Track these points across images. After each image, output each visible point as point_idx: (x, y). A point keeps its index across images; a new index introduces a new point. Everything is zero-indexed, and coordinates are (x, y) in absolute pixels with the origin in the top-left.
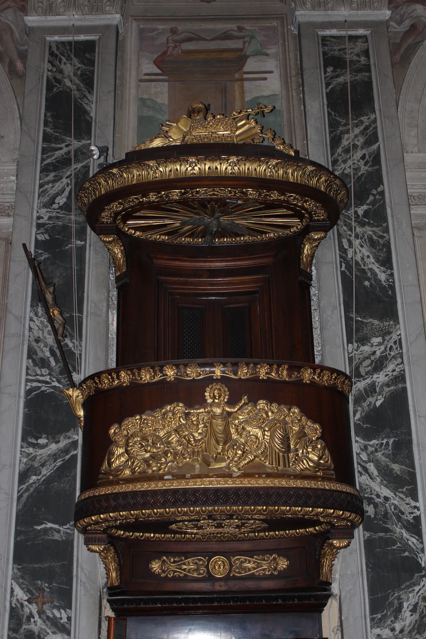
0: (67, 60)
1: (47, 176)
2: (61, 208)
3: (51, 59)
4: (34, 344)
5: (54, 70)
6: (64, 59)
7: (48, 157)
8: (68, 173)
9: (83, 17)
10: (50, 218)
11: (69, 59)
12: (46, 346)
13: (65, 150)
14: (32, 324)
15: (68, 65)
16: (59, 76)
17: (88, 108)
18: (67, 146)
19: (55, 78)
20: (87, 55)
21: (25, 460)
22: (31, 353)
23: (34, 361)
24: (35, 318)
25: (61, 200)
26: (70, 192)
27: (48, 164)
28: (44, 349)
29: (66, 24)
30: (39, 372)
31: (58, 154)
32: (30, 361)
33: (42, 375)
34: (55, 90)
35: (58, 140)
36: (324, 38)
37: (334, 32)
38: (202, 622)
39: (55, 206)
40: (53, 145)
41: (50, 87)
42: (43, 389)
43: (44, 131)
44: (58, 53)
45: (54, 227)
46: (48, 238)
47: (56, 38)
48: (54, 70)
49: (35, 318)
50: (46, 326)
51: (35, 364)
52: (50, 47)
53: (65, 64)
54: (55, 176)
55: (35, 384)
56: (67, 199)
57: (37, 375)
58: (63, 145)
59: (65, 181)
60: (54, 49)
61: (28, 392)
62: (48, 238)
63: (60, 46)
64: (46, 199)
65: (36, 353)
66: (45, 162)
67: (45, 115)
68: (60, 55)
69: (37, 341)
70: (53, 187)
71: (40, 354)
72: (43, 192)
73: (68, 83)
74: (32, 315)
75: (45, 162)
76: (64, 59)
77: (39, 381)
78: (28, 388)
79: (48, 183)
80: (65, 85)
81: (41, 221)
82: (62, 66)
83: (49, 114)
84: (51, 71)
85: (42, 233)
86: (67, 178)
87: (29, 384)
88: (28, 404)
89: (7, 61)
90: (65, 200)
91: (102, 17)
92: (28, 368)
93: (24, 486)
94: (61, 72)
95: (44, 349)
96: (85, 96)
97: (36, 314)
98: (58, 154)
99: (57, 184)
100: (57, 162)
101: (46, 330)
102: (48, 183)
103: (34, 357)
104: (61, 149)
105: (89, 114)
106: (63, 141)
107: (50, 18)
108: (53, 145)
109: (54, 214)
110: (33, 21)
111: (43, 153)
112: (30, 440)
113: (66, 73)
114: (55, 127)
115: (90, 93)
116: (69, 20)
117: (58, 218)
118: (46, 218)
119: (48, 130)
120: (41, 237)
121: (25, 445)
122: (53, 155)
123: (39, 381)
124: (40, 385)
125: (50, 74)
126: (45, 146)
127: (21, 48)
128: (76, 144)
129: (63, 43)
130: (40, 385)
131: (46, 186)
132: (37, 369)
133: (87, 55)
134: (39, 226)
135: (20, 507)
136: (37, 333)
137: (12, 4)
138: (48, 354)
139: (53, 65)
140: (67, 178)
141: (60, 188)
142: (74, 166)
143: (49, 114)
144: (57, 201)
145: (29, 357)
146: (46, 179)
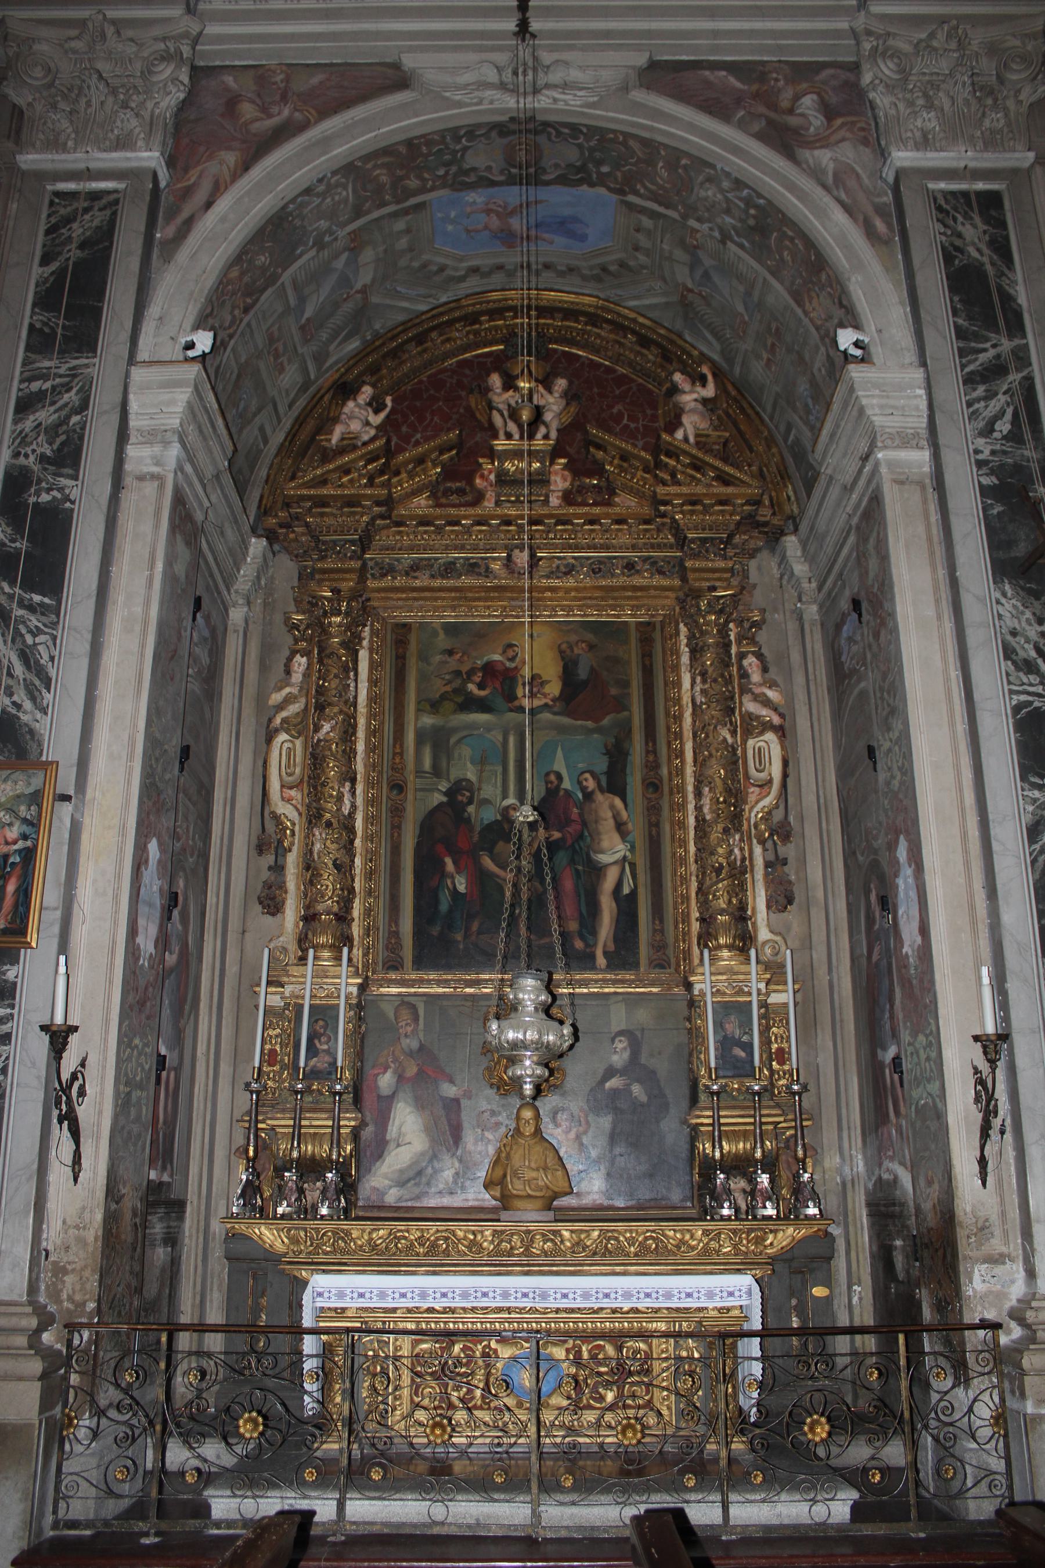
0: (965, 218)
1: (975, 390)
2: (1004, 438)
3: (940, 216)
4: (1009, 638)
5: (949, 232)
6: (960, 219)
7: (970, 362)
8: (1005, 387)
9: (979, 155)
10: (993, 453)
11: (967, 217)
12: (1028, 641)
13: (992, 353)
14: (1000, 608)
15: (968, 226)
16: (958, 242)
17: (1012, 291)
18: (994, 346)
19: (952, 244)
20: (993, 213)
21: (1030, 808)
22: (1008, 652)
23: (1014, 663)
24: (1003, 601)
25: (1003, 427)
26: (1016, 415)
27: (972, 373)
28: (1026, 646)
29: (954, 164)
30: (1025, 680)
31: (983, 357)
32: (1009, 663)
33: (1031, 685)
34: (957, 262)
35: (977, 337)
36: (57, 194)
37: (71, 186)
38: (116, 554)
39: (996, 435)
40: (973, 344)
41: (948, 258)
42: (1036, 704)
43: (955, 323)
44: (948, 207)
45: (1002, 466)
46: (996, 482)
47: (942, 185)
48: (949, 232)
49: (1003, 601)
50: (1023, 613)
51: (1018, 668)
52: (935, 199)
53: (963, 224)
54: (986, 391)
55: (1023, 698)
56: (1012, 424)
57: (1023, 684)
58: (988, 345)
59: (1002, 398)
60: (942, 202)
61: (1017, 709)
62: (996, 482)
63: (949, 197)
64: (981, 424)
65: (1014, 651)
66: (967, 370)
67: (951, 301)
68: (952, 212)
69: (1014, 633)
70: (986, 407)
71: (1022, 654)
72: (973, 413)
73: (975, 254)
74: (998, 595)
75: (967, 370)
76: (960, 219)
77: (1029, 693)
78: (1014, 703)
79: (978, 400)
80: (969, 256)
81: (980, 457)
82: (960, 228)
83: (956, 299)
84: (944, 234)
85: (987, 475)
86: (1005, 393)
87: (1015, 697)
88: (1020, 726)
89: (861, 218)
90: (1008, 427)
91: (1008, 155)
92: (1008, 674)
93: (1037, 846)
94: (960, 236)
95: (1026, 646)
96: (1003, 274)
97: (1004, 595)
98: (983, 357)
99: (993, 402)
100: (985, 369)
101: (1023, 619)
102: (978, 400)
103: (1014, 657)
104: (985, 350)
105: (1015, 300)
106: (987, 340)
107: (930, 155)
108: (973, 344)
109: (998, 447)
110: (906, 159)
111: (960, 357)
112: (1032, 779)
113: (968, 239)
114: (970, 318)
115: (1009, 269)
116: (959, 159)
117: (1004, 453)
118: (987, 452)
119: (960, 321)
120: (986, 481)
121: (1026, 786)
122: (976, 359)
123: (1029, 693)
124: (1030, 698)
125: (944, 238)
126: (961, 345)
127: (877, 200)
128: (1007, 345)
129: (953, 193)
130: (1030, 698)
131: (976, 406)
132: (1021, 674)
133: (993, 213)
134: (980, 464)
135: (1037, 877)
136: (1011, 623)
137: (848, 135)
138: (1033, 654)
139: (945, 226)
140: (1005, 393)
141: (998, 408)
142: (1011, 378)
143: (956, 299)
144: (997, 427)
145: (1007, 657)
146: (975, 395)
